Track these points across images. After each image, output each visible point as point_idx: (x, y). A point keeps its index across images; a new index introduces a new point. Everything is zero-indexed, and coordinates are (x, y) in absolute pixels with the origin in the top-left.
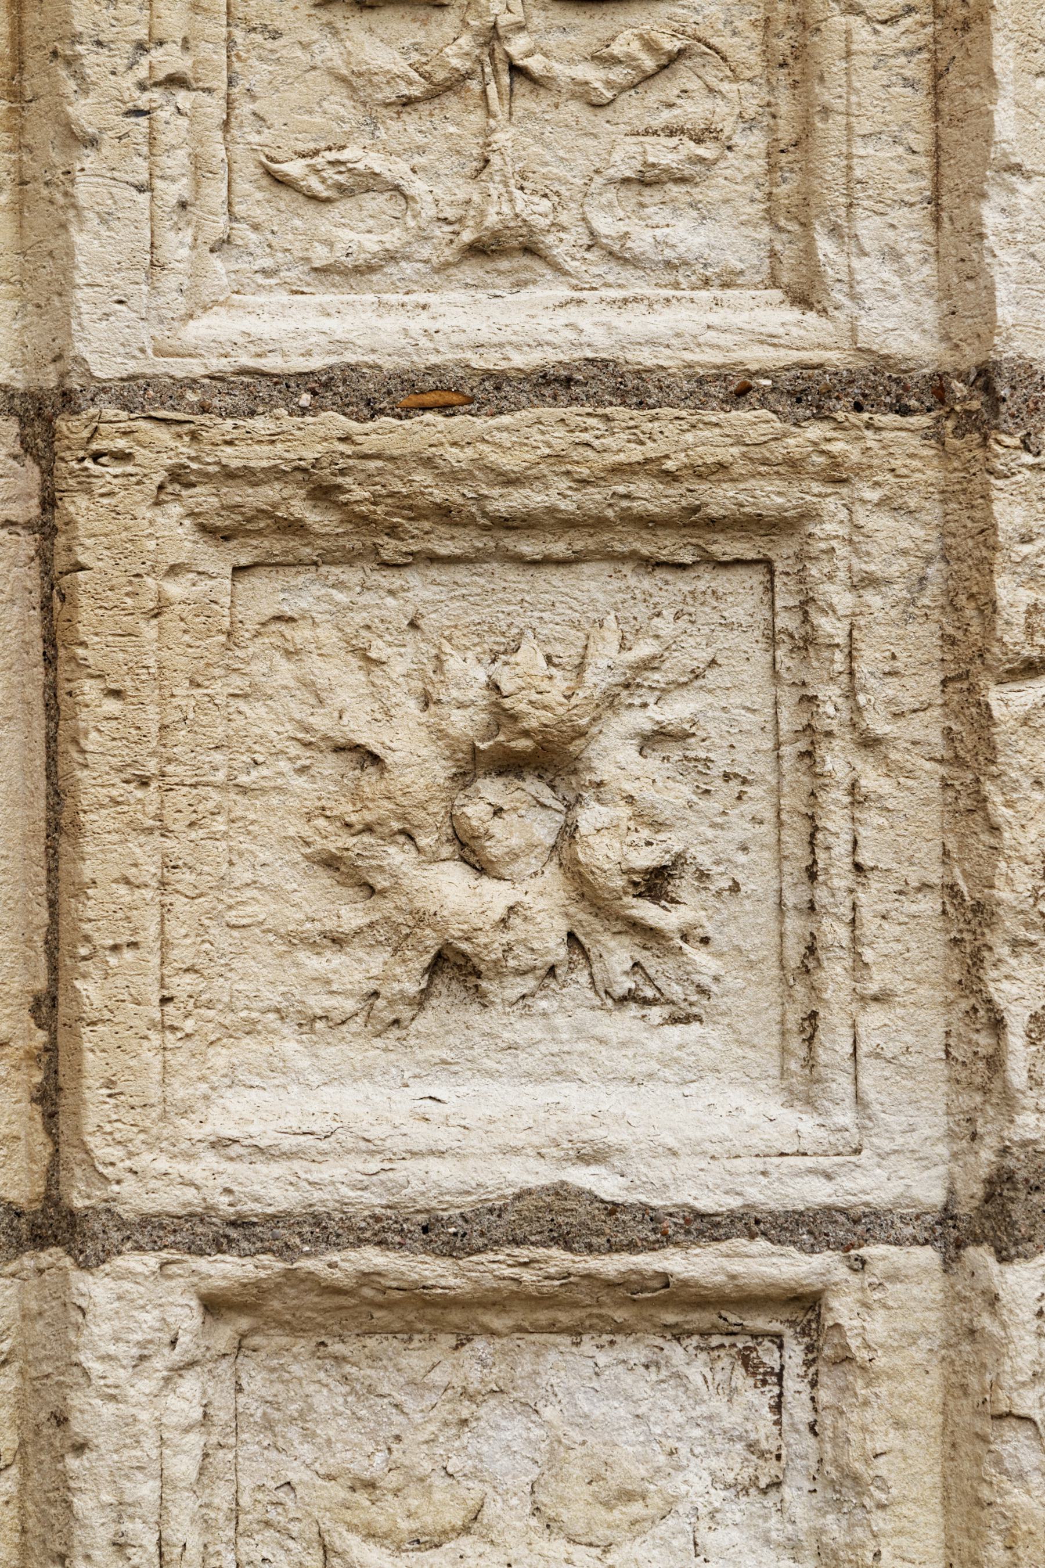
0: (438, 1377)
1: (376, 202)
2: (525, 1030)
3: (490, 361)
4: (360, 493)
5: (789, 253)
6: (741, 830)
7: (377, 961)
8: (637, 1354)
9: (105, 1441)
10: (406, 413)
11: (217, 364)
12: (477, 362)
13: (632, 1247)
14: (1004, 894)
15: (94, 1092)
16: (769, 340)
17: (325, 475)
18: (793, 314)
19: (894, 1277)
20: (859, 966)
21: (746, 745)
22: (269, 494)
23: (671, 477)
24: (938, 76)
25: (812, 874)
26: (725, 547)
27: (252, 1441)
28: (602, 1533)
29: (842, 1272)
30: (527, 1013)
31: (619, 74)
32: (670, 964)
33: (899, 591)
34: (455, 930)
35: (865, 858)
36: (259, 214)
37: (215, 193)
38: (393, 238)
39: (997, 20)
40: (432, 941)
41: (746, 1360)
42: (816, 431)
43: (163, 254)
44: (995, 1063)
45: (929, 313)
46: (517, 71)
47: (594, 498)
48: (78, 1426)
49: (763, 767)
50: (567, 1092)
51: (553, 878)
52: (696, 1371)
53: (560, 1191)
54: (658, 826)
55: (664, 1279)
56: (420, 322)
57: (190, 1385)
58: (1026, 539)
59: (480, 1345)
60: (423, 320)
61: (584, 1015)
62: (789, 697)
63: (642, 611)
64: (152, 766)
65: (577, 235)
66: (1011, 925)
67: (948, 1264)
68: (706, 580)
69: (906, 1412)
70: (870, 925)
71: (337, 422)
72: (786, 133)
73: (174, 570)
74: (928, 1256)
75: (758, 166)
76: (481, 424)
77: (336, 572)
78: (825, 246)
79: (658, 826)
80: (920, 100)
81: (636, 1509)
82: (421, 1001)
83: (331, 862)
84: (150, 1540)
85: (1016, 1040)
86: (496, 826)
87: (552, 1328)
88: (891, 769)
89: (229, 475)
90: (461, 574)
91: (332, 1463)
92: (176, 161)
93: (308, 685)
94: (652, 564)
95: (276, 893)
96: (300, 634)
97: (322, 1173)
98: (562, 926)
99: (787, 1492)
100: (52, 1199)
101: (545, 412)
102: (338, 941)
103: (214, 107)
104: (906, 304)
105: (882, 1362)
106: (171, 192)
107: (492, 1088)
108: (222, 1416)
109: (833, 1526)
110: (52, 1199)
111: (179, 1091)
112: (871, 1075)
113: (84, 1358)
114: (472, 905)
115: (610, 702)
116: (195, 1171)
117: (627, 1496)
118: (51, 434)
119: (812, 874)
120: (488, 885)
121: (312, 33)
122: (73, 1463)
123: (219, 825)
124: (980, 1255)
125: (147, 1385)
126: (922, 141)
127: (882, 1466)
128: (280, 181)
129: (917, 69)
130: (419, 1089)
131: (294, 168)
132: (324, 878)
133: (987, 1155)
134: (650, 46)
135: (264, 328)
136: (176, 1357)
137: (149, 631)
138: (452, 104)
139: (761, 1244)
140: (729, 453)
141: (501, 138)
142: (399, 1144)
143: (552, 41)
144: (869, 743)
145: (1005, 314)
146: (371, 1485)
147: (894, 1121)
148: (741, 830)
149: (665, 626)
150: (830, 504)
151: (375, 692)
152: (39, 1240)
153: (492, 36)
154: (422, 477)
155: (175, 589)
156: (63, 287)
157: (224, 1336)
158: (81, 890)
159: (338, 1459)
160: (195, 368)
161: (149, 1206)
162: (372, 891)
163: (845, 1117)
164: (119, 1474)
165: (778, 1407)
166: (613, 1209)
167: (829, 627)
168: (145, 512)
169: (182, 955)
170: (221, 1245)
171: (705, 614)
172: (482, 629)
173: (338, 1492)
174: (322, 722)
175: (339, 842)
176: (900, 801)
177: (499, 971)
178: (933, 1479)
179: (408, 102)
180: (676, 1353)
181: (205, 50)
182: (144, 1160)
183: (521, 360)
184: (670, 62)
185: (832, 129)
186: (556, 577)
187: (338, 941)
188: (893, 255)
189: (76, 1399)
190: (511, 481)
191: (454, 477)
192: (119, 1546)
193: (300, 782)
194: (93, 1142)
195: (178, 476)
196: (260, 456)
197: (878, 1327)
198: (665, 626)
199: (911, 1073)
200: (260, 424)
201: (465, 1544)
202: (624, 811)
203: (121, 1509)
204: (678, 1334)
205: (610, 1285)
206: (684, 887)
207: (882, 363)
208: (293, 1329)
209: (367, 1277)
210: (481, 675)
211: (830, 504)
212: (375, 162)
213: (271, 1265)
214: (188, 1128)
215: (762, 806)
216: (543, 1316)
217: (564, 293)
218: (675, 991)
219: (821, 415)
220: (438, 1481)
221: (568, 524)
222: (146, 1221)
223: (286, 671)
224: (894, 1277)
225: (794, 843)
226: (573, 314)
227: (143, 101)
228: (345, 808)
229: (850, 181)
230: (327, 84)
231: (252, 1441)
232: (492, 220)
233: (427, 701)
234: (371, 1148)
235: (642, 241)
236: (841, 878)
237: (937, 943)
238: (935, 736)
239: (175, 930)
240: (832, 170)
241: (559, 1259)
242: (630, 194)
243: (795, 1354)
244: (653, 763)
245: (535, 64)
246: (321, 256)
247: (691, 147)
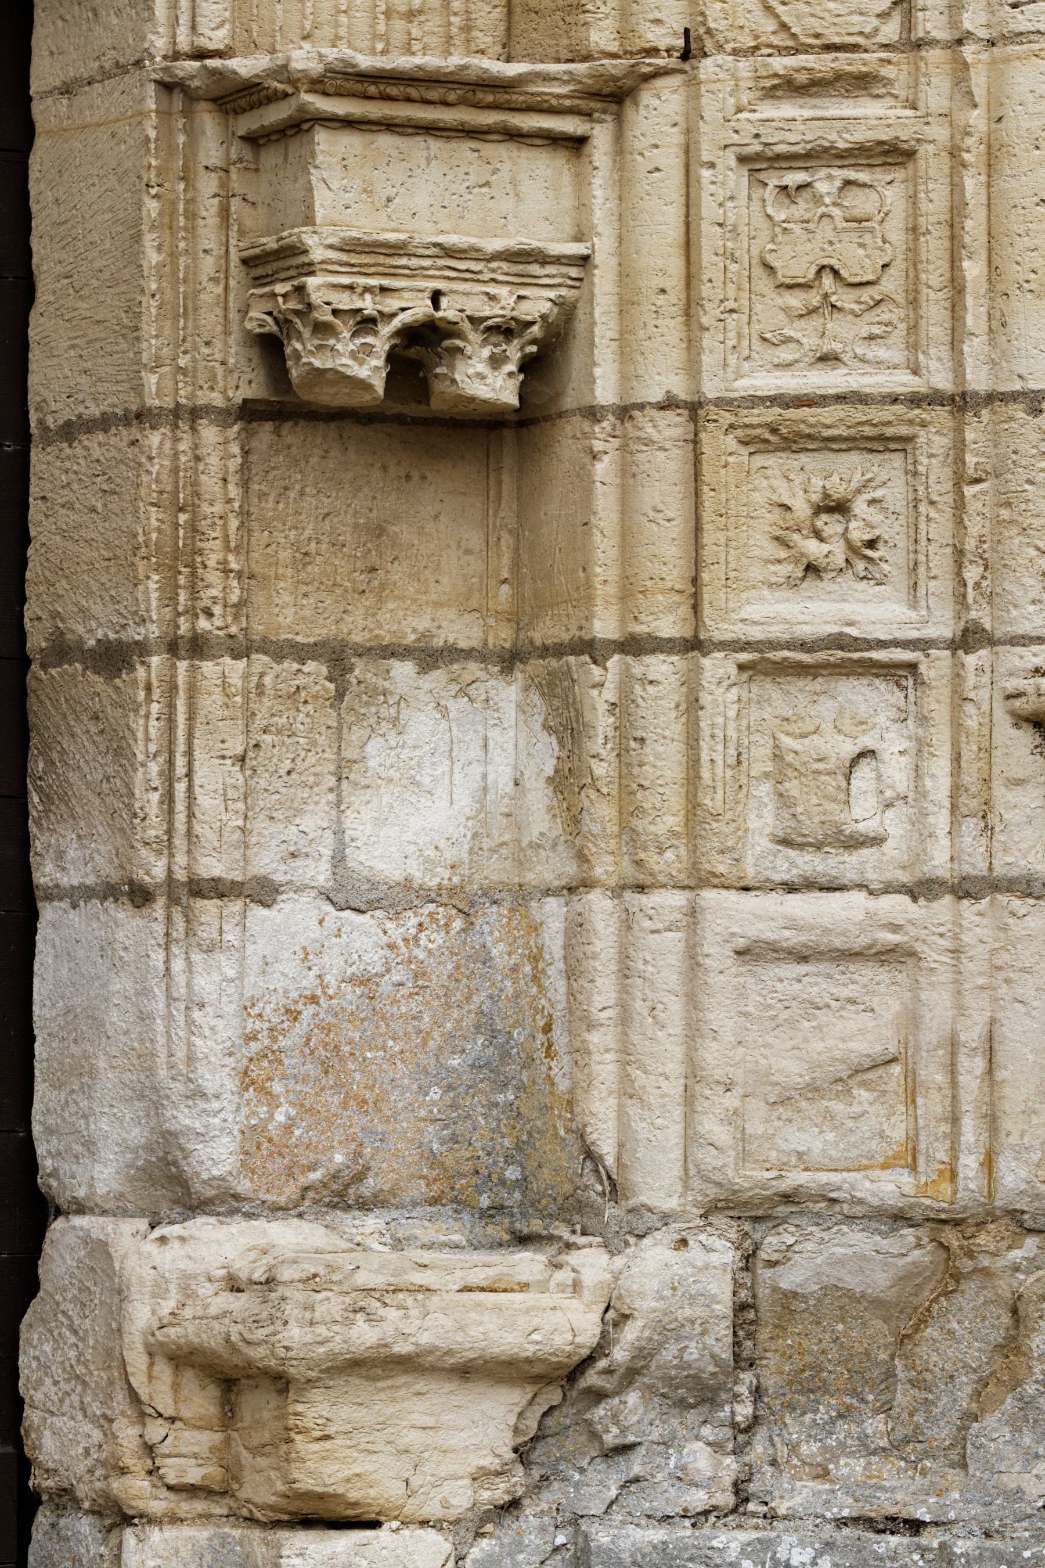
0: (807, 688)
1: (792, 345)
2: (834, 587)
3: (822, 392)
4: (784, 431)
5: (912, 359)
6: (897, 528)
7: (790, 567)
8: (865, 682)
9: (708, 706)
10: (798, 407)
11: (743, 394)
12: (818, 392)
13: (861, 650)
14: (967, 547)
15: (706, 606)
16: (904, 385)
17: (774, 425)
18: (911, 377)
19: (938, 659)
20: (929, 568)
21: (899, 504)
22: (758, 431)
23: (875, 425)
24: (953, 306)
25: (916, 541)
26: (892, 446)
27: (754, 707)
28: (854, 734)
29: (922, 658)
30: (834, 582)
31: (863, 307)
32: (876, 568)
33: (941, 458)
34: (812, 558)
35: (930, 536)
36: (759, 349)
37: (745, 343)
38: (797, 356)
39: (968, 290)
40: (805, 561)
41: (897, 684)
42: (917, 411)
43: (728, 362)
44: (964, 596)
45: (950, 376)
46: (833, 306)
47: (852, 432)
48: (702, 702)
49: (903, 510)
50: (846, 606)
51: (842, 542)
52: (883, 686)
53: (841, 634)
54: (873, 527)
55: (871, 659)
56: (801, 381)
57: (734, 690)
58: (975, 443)
59: (820, 679)
60: (805, 380)
61: (851, 583)
62: (911, 489)
63: (868, 464)
64: (723, 511)
65: (851, 354)
66: (969, 556)
67: (953, 655)
68: (887, 456)
69: (941, 698)
70: (932, 557)
71: (777, 410)
72: (912, 323)
73: (730, 454)
74: (947, 653)
75: (905, 333)
76: (819, 410)
77: (779, 454)
78: (921, 357)
79: (873, 527)
80: (948, 313)
81: (864, 727)
82: (803, 579)
83: (777, 539)
84: (721, 735)
85: (970, 590)
86: (826, 528)
87: (841, 674)
88: (939, 511)
89: (746, 426)
90: (816, 454)
91: (777, 713)
92: (732, 334)
93: (771, 487)
94: (871, 451)
95: (762, 548)
96: (769, 472)
97: (772, 629)
98: (844, 557)
99: (909, 722)
100: (696, 636)
101: (839, 407)
102: (779, 561)
103: (745, 318)
104: (943, 374)
105: (934, 684)
106: (730, 343)
107: (824, 604)
108: (745, 699)
109: (920, 731)
110: (696, 636)
111: (731, 605)
112: (932, 600)
113: (704, 683)
114: (817, 551)
115: (859, 491)
116: (735, 628)
117: (862, 723)
118: (696, 414)
119: (916, 541)
120: (823, 545)
121: (774, 295)
122: (700, 713)
123: (744, 528)
124: (960, 652)
125: (721, 690)
126: (948, 325)
127: (933, 714)
128: (765, 340)
129: (947, 304)
130: (802, 605)
131: (768, 336)
132: (776, 543)
133: (963, 623)
134: (872, 298)
135: (757, 383)
136: (729, 682)
137: (723, 471)
138: (814, 315)
139: (899, 650)
140: (890, 418)
141: (829, 326)
142: (794, 621)
143: (844, 297)
144: (932, 503)
145: (969, 377)
146: (787, 720)
147: (938, 614)
148: (897, 528)
149: (875, 469)
150: (922, 433)
151: (791, 489)
152: (693, 649)
153: (826, 296)
154: (802, 426)
155: (731, 459)
156: (699, 372)
157: (745, 676)
158: (703, 547)
159: (779, 712)
160: (736, 395)
161: (722, 639)
162: (789, 547)
163: (924, 612)
164: (712, 716)
165: (906, 697)
166: (856, 639)
167: (921, 469)
168: (722, 437)
169: (732, 565)
170: (742, 649)
171: (887, 465)
172: (821, 470)
173: (778, 721)
174: (775, 498)
175: (779, 533)
176: (941, 520)
177: (825, 570)
178: (948, 718)
179: (802, 316)
180: (877, 681)
181: (742, 301)
182: (720, 625)
183: (831, 391)
184: (878, 303)
185: (923, 322)
186: (844, 455)
187: (779, 561)
188: (940, 359)
189: (701, 694)
190: (828, 427)
191: (811, 426)
192: (713, 736)
193: (768, 515)
194: (706, 620)
195: (732, 426)
196: (755, 421)
197: (932, 673)
198: (875, 469)
199: (943, 599)
200: (755, 411)
201: (815, 737)
202: (863, 523)
203: (713, 726)
204: (877, 676)
205: (855, 661)
206: (880, 545)
207: (937, 391)
208: (767, 674)
209: (785, 659)
210: (821, 484)
211: (922, 433)
212: (792, 333)
213: (756, 656)
214: (734, 616)
215: (902, 520)
216: (837, 671)
217: (846, 371)
218: (878, 576)
219: (919, 407)
220: (807, 718)
221: (846, 439)
222: (721, 643)
223: (765, 483)
224: (938, 659)
225: (912, 533)
226: (848, 378)
227: (722, 317)
228: (781, 523)
229: (928, 338)
230: (779, 311)
231: (754, 707)
232: (825, 350)
233: (806, 491)
234: (786, 622)
235: (870, 355)
236: (923, 542)
237: (951, 561)
238: (951, 501)
239: (730, 558)
240: (923, 334)
241: (840, 654)
242: (866, 342)
243: (911, 682)
244: (872, 509)
245: (838, 304)
246: (776, 361)
247: (884, 328)
